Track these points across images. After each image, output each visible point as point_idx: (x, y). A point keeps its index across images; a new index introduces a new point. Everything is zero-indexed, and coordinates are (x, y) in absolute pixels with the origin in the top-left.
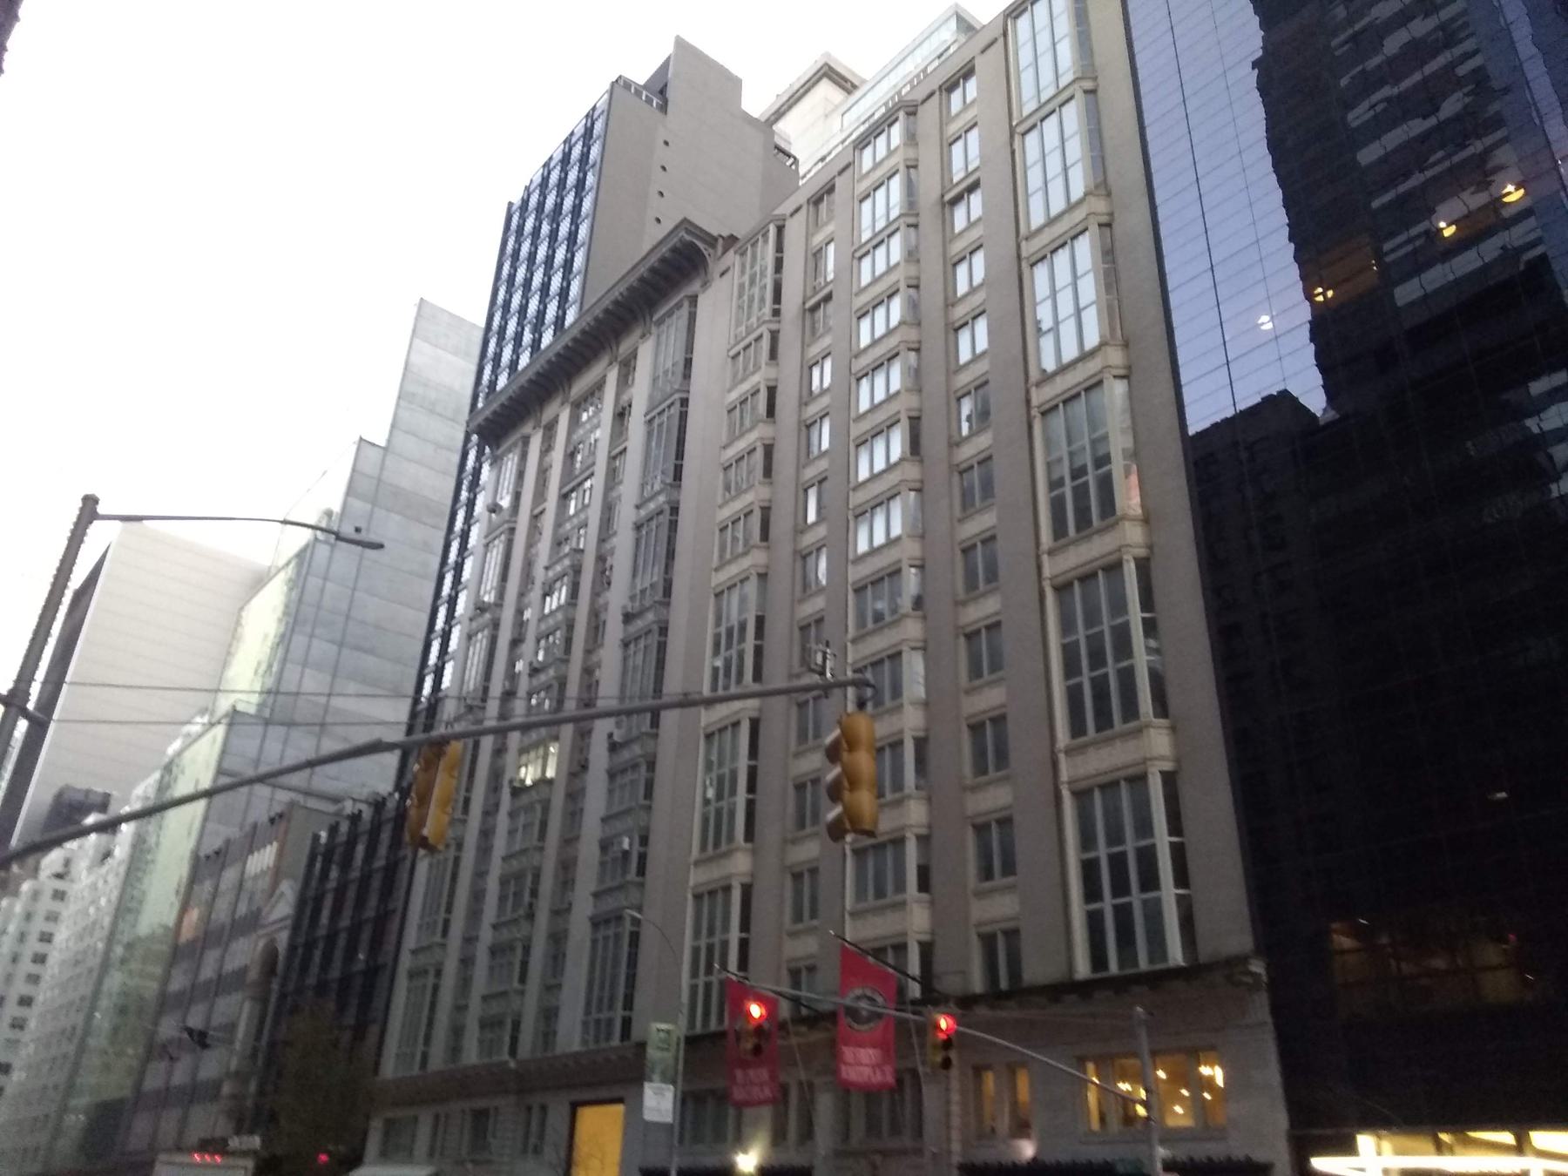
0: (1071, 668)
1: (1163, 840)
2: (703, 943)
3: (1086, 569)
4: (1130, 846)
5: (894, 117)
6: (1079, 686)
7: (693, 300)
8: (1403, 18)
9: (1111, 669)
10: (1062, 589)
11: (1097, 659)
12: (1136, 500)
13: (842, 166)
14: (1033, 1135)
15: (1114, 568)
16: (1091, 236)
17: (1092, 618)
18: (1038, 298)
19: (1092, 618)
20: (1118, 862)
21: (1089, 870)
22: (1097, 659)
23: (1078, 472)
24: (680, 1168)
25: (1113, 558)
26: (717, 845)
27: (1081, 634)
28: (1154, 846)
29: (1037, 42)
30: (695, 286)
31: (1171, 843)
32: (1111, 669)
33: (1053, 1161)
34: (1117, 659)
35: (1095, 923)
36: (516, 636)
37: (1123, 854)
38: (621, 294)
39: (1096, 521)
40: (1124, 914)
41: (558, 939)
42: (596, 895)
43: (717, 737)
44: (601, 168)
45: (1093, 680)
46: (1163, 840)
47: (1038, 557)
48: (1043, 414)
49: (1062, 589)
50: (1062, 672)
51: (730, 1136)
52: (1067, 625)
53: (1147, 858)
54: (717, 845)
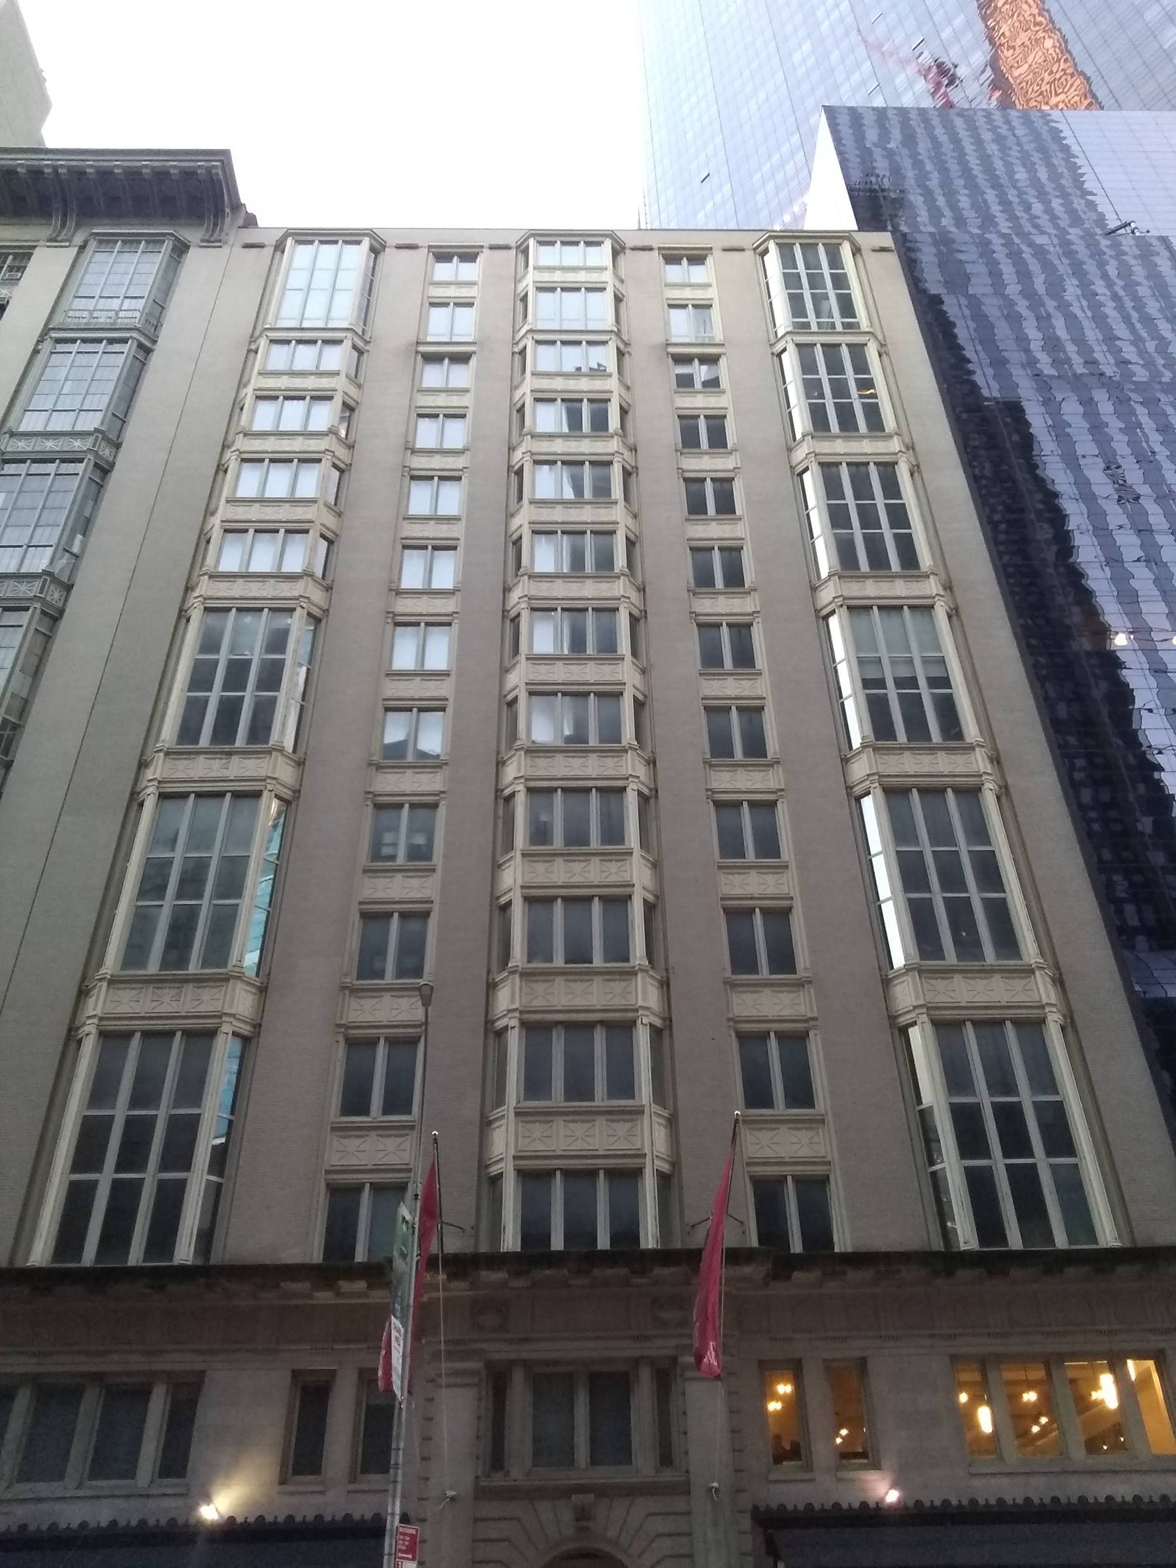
3: (160, 1025)
5: (600, 239)
7: (181, 249)
9: (150, 1177)
11: (134, 1154)
12: (251, 958)
13: (501, 242)
14: (885, 1463)
16: (840, 617)
17: (145, 1094)
18: (845, 663)
19: (145, 1094)
22: (134, 1154)
23: (192, 881)
24: (385, 1470)
27: (120, 1111)
30: (192, 235)
32: (150, 1177)
33: (828, 1505)
34: (164, 1166)
36: (514, 708)
45: (117, 1185)
52: (102, 1091)
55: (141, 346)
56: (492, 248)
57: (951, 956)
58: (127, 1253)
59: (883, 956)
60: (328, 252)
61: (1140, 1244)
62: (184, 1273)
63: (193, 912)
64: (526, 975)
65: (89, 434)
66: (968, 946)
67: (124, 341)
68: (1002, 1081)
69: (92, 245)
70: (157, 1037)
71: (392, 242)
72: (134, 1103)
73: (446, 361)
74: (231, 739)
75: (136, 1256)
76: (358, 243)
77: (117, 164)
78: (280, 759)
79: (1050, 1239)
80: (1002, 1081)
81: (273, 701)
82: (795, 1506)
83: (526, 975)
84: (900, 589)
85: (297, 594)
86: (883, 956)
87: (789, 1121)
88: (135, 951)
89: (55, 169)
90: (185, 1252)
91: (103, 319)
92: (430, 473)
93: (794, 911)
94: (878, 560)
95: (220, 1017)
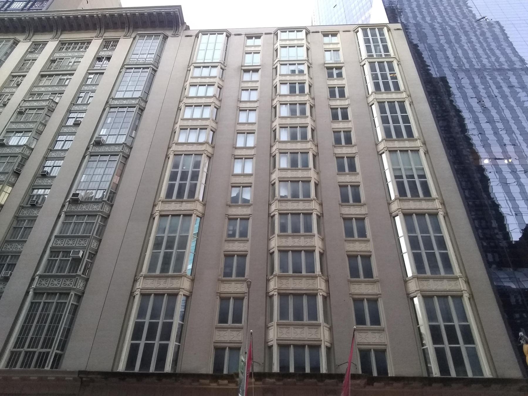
0: (137, 335)
1: (176, 321)
4: (161, 321)
6: (138, 345)
8: (520, 185)
10: (145, 296)
11: (151, 335)
15: (173, 296)
17: (155, 315)
19: (155, 315)
20: (153, 327)
21: (138, 328)
22: (151, 335)
25: (176, 291)
27: (147, 320)
28: (168, 345)
29: (215, 53)
30: (169, 33)
34: (161, 339)
35: (134, 349)
37: (174, 237)
38: (97, 15)
39: (185, 197)
40: (149, 348)
43: (10, 265)
44: (9, 120)
46: (176, 321)
48: (161, 216)
49: (145, 296)
50: (131, 337)
51: (148, 17)
52: (141, 313)
53: (168, 327)
55: (153, 70)
56: (266, 34)
57: (429, 273)
61: (500, 377)
64: (280, 277)
65: (137, 98)
66: (434, 267)
67: (148, 68)
68: (448, 317)
69: (138, 37)
73: (251, 71)
76: (222, 34)
77: (137, 12)
79: (450, 374)
80: (448, 317)
83: (280, 277)
84: (407, 144)
87: (372, 330)
89: (126, 13)
91: (141, 61)
93: (372, 256)
94: (399, 134)
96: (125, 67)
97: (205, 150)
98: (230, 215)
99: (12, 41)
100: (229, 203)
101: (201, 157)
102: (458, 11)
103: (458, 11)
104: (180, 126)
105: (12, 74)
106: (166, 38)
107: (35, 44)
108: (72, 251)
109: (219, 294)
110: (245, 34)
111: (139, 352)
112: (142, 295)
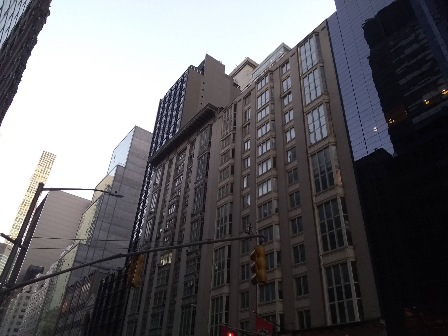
2: (215, 314)
4: (343, 284)
11: (331, 228)
17: (329, 215)
19: (329, 215)
22: (331, 228)
26: (218, 284)
27: (334, 286)
30: (212, 122)
31: (357, 299)
35: (333, 308)
40: (341, 306)
41: (171, 312)
42: (183, 299)
47: (312, 197)
53: (348, 287)
54: (218, 284)
58: (346, 320)
59: (242, 184)
60: (307, 44)
62: (358, 324)
63: (343, 303)
70: (327, 203)
71: (320, 30)
72: (327, 218)
74: (327, 187)
75: (348, 321)
76: (312, 37)
78: (338, 187)
81: (332, 173)
82: (50, 7)
85: (227, 200)
86: (242, 184)
88: (325, 249)
90: (358, 318)
92: (320, 149)
95: (346, 259)
96: (302, 77)
97: (271, 175)
98: (292, 217)
99: (209, 126)
100: (290, 209)
101: (329, 149)
102: (149, 171)
103: (149, 171)
104: (272, 155)
105: (243, 126)
106: (211, 125)
107: (192, 143)
108: (157, 305)
109: (294, 277)
110: (279, 66)
111: (345, 307)
112: (326, 269)
